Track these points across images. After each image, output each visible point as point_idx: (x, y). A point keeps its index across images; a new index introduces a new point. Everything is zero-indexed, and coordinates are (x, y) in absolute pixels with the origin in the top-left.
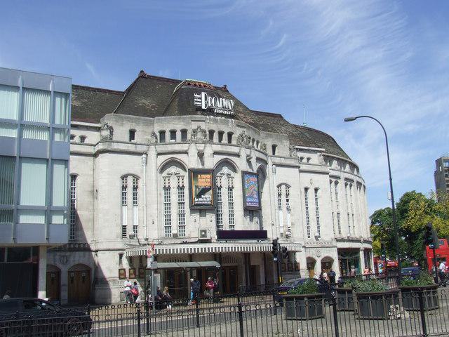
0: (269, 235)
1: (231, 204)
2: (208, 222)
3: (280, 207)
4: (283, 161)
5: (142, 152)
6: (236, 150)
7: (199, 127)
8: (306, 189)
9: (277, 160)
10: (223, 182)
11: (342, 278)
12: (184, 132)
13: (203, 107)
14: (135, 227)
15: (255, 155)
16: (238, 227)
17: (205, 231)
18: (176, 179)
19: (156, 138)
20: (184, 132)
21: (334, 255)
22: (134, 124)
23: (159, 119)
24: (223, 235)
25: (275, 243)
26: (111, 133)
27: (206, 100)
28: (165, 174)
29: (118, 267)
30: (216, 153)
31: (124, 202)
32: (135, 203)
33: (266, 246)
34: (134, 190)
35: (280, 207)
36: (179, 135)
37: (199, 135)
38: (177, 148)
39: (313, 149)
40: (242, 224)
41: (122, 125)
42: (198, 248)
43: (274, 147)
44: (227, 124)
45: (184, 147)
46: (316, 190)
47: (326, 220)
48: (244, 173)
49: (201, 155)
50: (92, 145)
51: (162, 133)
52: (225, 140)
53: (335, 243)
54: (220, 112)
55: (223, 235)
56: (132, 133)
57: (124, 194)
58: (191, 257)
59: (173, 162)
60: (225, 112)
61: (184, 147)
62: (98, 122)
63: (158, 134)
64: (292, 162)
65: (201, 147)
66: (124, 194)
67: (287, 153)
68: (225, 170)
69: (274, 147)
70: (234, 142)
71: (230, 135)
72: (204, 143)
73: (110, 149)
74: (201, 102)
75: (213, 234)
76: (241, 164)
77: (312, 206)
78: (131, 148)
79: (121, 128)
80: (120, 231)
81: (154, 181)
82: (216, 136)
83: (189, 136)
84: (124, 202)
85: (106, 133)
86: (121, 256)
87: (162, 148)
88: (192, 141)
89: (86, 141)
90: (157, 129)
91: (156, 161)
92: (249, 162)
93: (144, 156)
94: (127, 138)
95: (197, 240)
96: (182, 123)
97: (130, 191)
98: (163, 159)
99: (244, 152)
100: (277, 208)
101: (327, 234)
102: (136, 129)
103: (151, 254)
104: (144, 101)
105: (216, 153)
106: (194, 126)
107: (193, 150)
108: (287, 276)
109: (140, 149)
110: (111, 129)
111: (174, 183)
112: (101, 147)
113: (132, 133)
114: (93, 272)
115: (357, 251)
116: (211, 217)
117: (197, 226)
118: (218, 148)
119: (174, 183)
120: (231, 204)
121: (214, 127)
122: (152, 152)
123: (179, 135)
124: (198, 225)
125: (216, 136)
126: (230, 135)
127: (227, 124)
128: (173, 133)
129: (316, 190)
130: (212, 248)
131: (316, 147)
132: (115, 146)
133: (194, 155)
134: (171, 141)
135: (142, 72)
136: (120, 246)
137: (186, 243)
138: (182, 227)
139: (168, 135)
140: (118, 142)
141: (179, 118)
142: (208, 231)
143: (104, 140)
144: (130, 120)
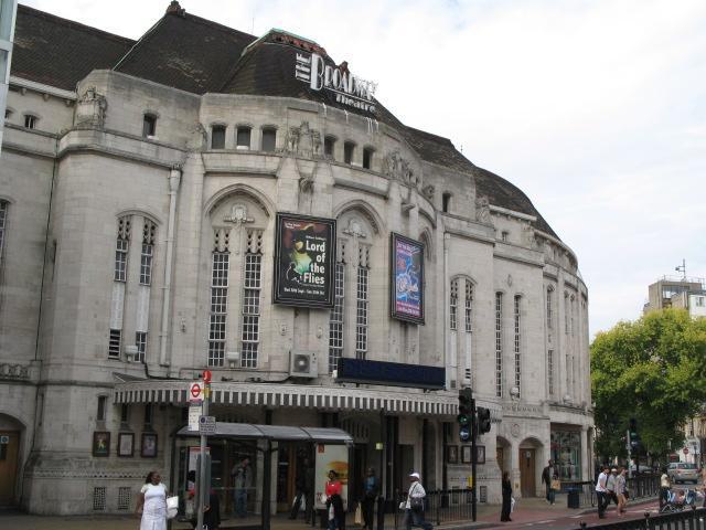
0: (450, 376)
1: (362, 306)
2: (313, 336)
3: (453, 326)
4: (464, 227)
5: (171, 164)
6: (380, 184)
7: (306, 124)
8: (499, 294)
9: (454, 224)
10: (350, 253)
11: (278, 512)
12: (269, 132)
13: (314, 86)
14: (141, 337)
15: (418, 201)
16: (376, 354)
17: (304, 358)
18: (244, 236)
19: (205, 137)
20: (269, 132)
21: (544, 435)
22: (156, 101)
23: (214, 98)
24: (355, 370)
25: (466, 398)
26: (103, 110)
27: (319, 71)
28: (218, 222)
29: (93, 426)
30: (339, 185)
31: (121, 277)
32: (145, 280)
33: (443, 401)
34: (144, 251)
35: (453, 326)
36: (256, 136)
37: (305, 141)
38: (253, 163)
39: (512, 212)
40: (385, 346)
41: (129, 98)
42: (319, 398)
43: (446, 197)
44: (364, 127)
45: (271, 164)
46: (517, 297)
47: (534, 363)
48: (395, 238)
49: (307, 186)
50: (51, 136)
51: (219, 130)
52: (357, 161)
53: (546, 411)
54: (349, 102)
55: (355, 370)
56: (150, 120)
57: (122, 256)
58: (268, 414)
59: (240, 194)
60: (358, 105)
61: (271, 164)
62: (73, 88)
63: (209, 131)
64: (483, 233)
65: (308, 168)
66: (122, 256)
67: (470, 213)
68: (358, 226)
69: (446, 197)
70: (375, 167)
71: (368, 153)
72: (315, 159)
73: (95, 147)
74: (309, 74)
75: (321, 362)
76: (390, 218)
77: (509, 331)
78: (147, 151)
79: (126, 105)
80: (106, 342)
81: (193, 235)
82: (339, 151)
83: (279, 142)
84: (121, 277)
85: (87, 110)
86: (102, 399)
87: (216, 161)
88: (285, 153)
89: (39, 126)
90: (207, 116)
91: (199, 189)
92: (406, 214)
93: (175, 174)
94: (138, 127)
95: (284, 377)
96: (266, 112)
97: (135, 251)
98: (218, 185)
99: (397, 193)
100: (448, 326)
101: (535, 390)
102: (453, 191)
103: (202, 396)
104: (178, 61)
105: (339, 185)
106: (295, 120)
107: (289, 174)
108: (460, 472)
109: (166, 157)
110: (102, 102)
111: (237, 244)
112: (73, 140)
113: (150, 120)
114: (28, 436)
115: (578, 428)
116: (319, 325)
117: (289, 346)
118: (344, 174)
119: (237, 244)
120: (362, 306)
121: (335, 129)
122: (195, 169)
123: (256, 136)
124: (284, 337)
125: (339, 151)
126: (368, 153)
127: (364, 127)
128: (244, 132)
129: (517, 297)
130: (327, 398)
131: (519, 211)
132: (109, 142)
133: (292, 185)
134: (239, 147)
135: (175, 4)
136: (102, 377)
137: (259, 381)
138: (249, 349)
139: (230, 135)
140: (115, 133)
141: (261, 101)
142: (312, 359)
143: (84, 125)
144: (152, 92)
